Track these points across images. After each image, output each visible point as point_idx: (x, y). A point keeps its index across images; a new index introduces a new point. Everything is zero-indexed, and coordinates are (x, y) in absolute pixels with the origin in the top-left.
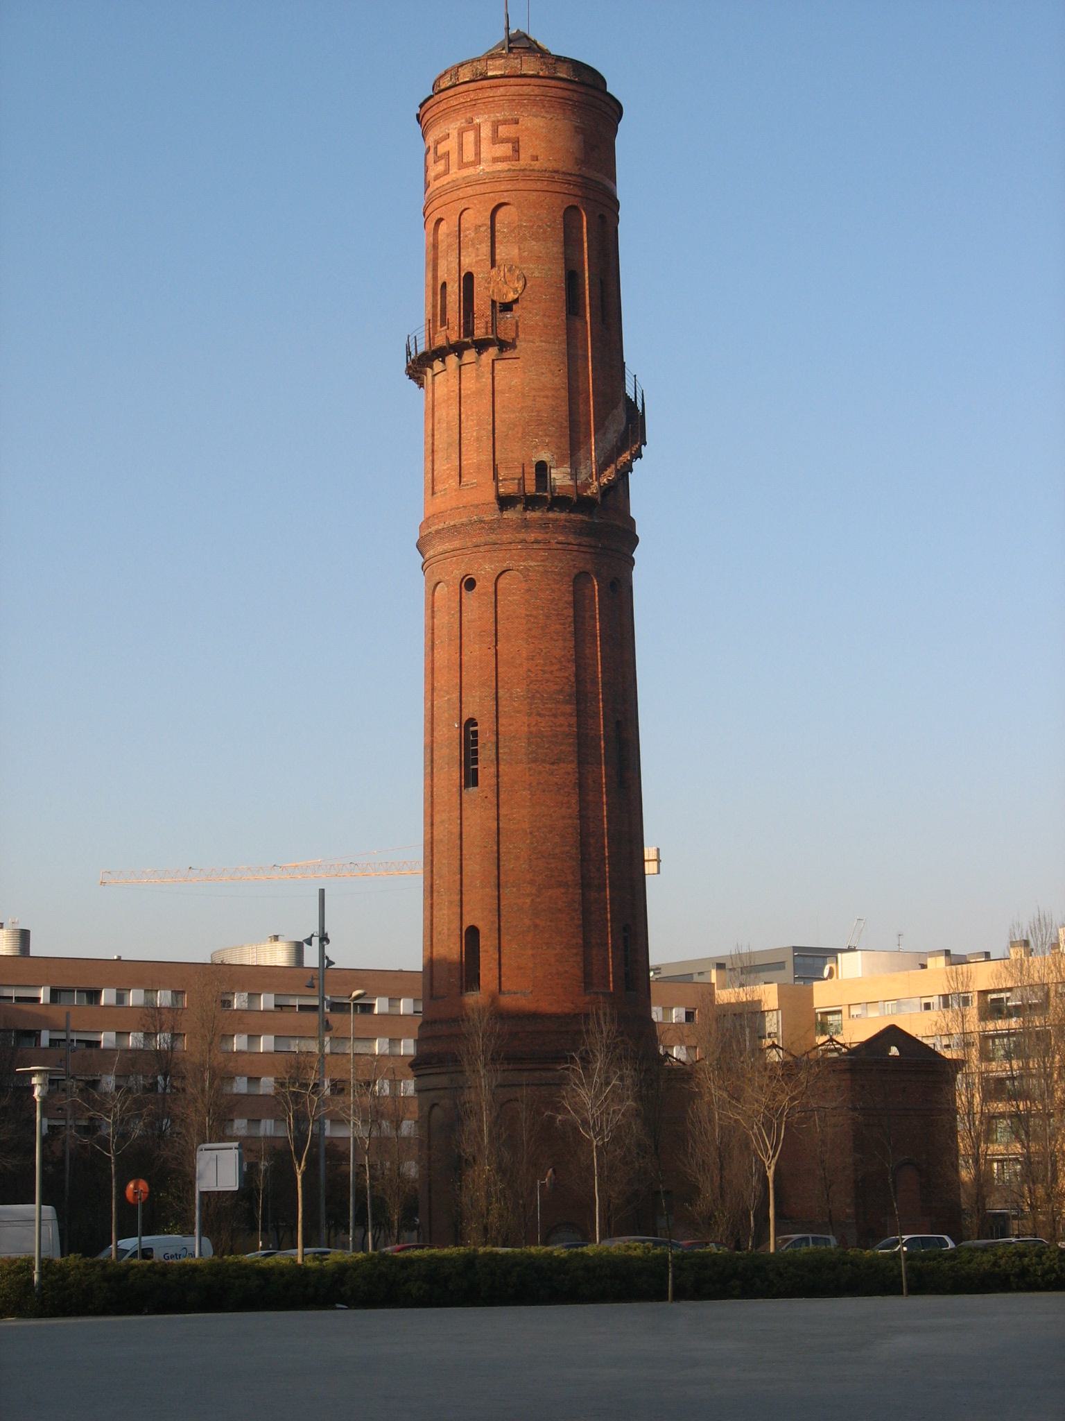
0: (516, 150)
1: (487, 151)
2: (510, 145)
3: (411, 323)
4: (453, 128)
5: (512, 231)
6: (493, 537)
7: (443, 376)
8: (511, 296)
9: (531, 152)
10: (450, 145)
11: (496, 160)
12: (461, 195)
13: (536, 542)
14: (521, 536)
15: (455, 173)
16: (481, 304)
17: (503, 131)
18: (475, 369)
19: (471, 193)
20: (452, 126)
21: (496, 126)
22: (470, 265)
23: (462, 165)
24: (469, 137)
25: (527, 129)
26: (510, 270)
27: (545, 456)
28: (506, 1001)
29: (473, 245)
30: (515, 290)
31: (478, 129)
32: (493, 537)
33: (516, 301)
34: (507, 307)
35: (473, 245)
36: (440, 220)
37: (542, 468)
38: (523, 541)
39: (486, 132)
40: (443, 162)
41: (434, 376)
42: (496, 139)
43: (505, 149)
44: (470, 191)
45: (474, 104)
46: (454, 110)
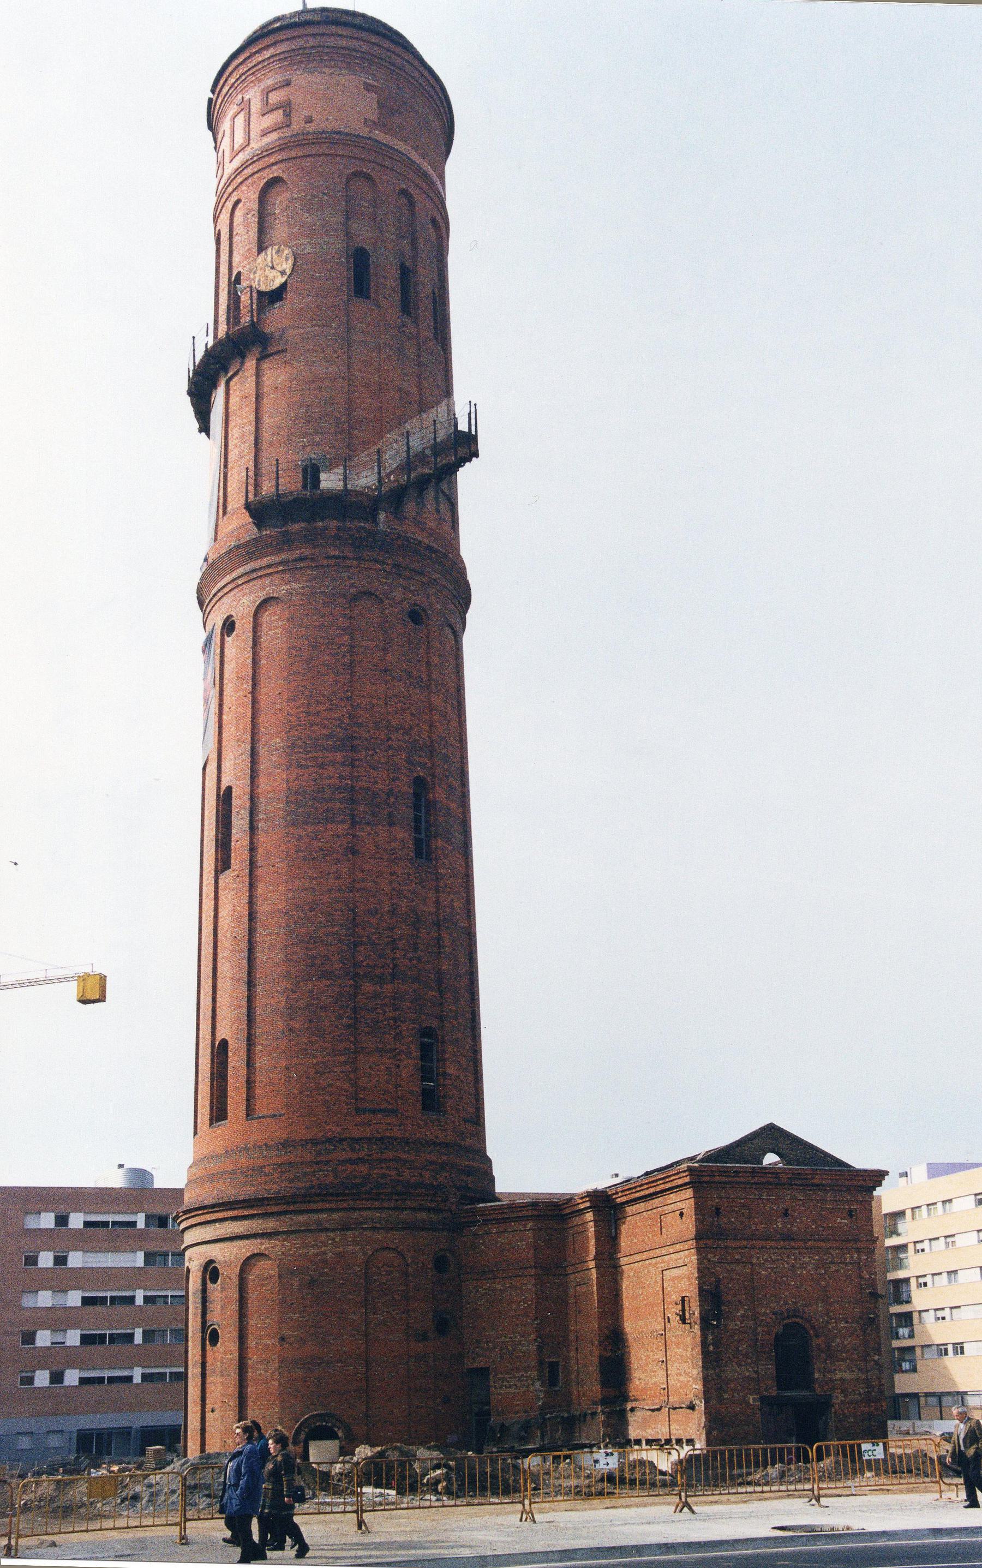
33: (284, 286)
37: (311, 473)
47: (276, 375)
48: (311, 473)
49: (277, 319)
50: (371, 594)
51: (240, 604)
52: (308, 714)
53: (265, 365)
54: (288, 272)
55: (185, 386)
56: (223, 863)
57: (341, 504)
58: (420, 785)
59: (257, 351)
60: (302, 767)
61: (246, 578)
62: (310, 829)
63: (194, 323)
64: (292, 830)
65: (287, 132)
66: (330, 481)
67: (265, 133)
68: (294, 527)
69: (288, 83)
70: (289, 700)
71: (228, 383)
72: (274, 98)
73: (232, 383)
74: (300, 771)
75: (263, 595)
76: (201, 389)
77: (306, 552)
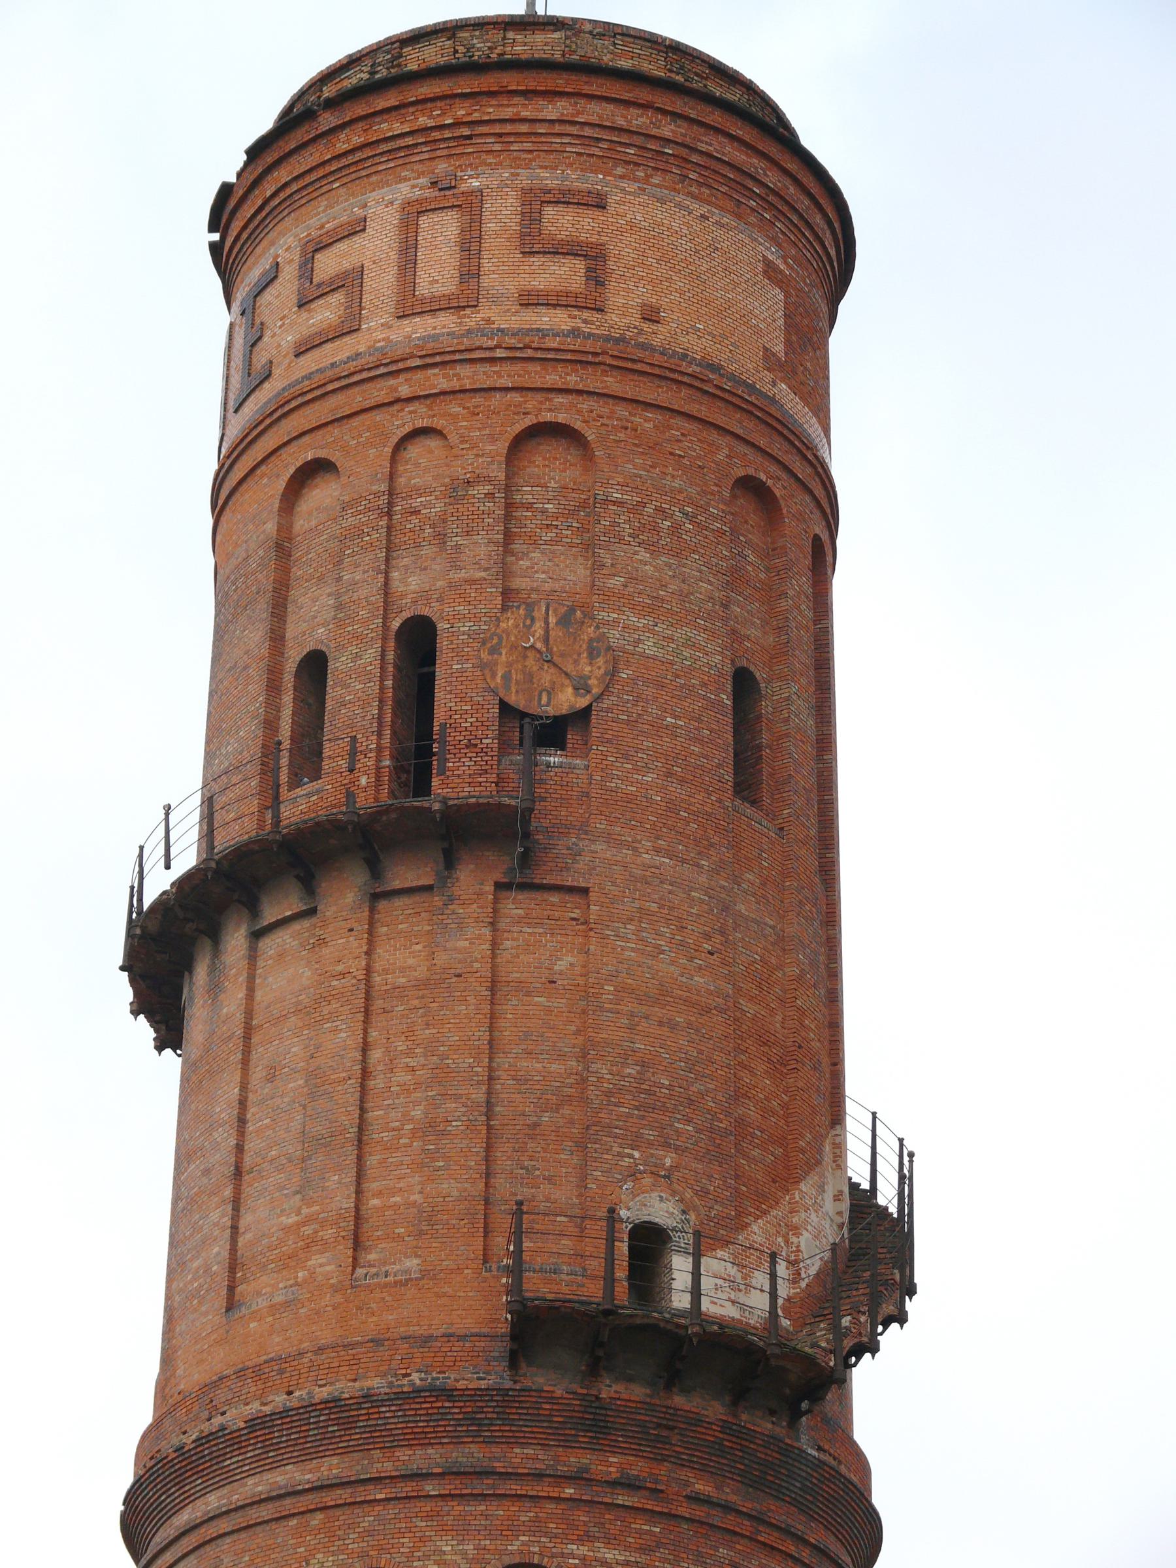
0: (596, 278)
1: (504, 272)
2: (579, 264)
3: (143, 783)
4: (382, 203)
5: (571, 513)
6: (471, 1454)
7: (279, 969)
8: (567, 700)
9: (642, 294)
10: (375, 248)
11: (529, 300)
12: (405, 391)
13: (629, 1484)
14: (576, 1460)
15: (383, 330)
16: (458, 700)
17: (559, 222)
18: (433, 939)
19: (443, 384)
20: (386, 193)
21: (535, 201)
22: (424, 596)
23: (410, 306)
24: (441, 233)
25: (632, 226)
26: (564, 621)
27: (660, 1209)
28: (537, 1287)
29: (441, 539)
30: (581, 687)
31: (471, 206)
32: (471, 1454)
33: (583, 716)
34: (553, 732)
35: (441, 539)
36: (315, 470)
37: (649, 1244)
38: (579, 1477)
39: (502, 216)
40: (337, 298)
41: (257, 935)
42: (533, 244)
43: (566, 274)
44: (440, 380)
45: (463, 137)
46: (397, 151)
59: (498, 865)
76: (165, 957)
77: (639, 1468)
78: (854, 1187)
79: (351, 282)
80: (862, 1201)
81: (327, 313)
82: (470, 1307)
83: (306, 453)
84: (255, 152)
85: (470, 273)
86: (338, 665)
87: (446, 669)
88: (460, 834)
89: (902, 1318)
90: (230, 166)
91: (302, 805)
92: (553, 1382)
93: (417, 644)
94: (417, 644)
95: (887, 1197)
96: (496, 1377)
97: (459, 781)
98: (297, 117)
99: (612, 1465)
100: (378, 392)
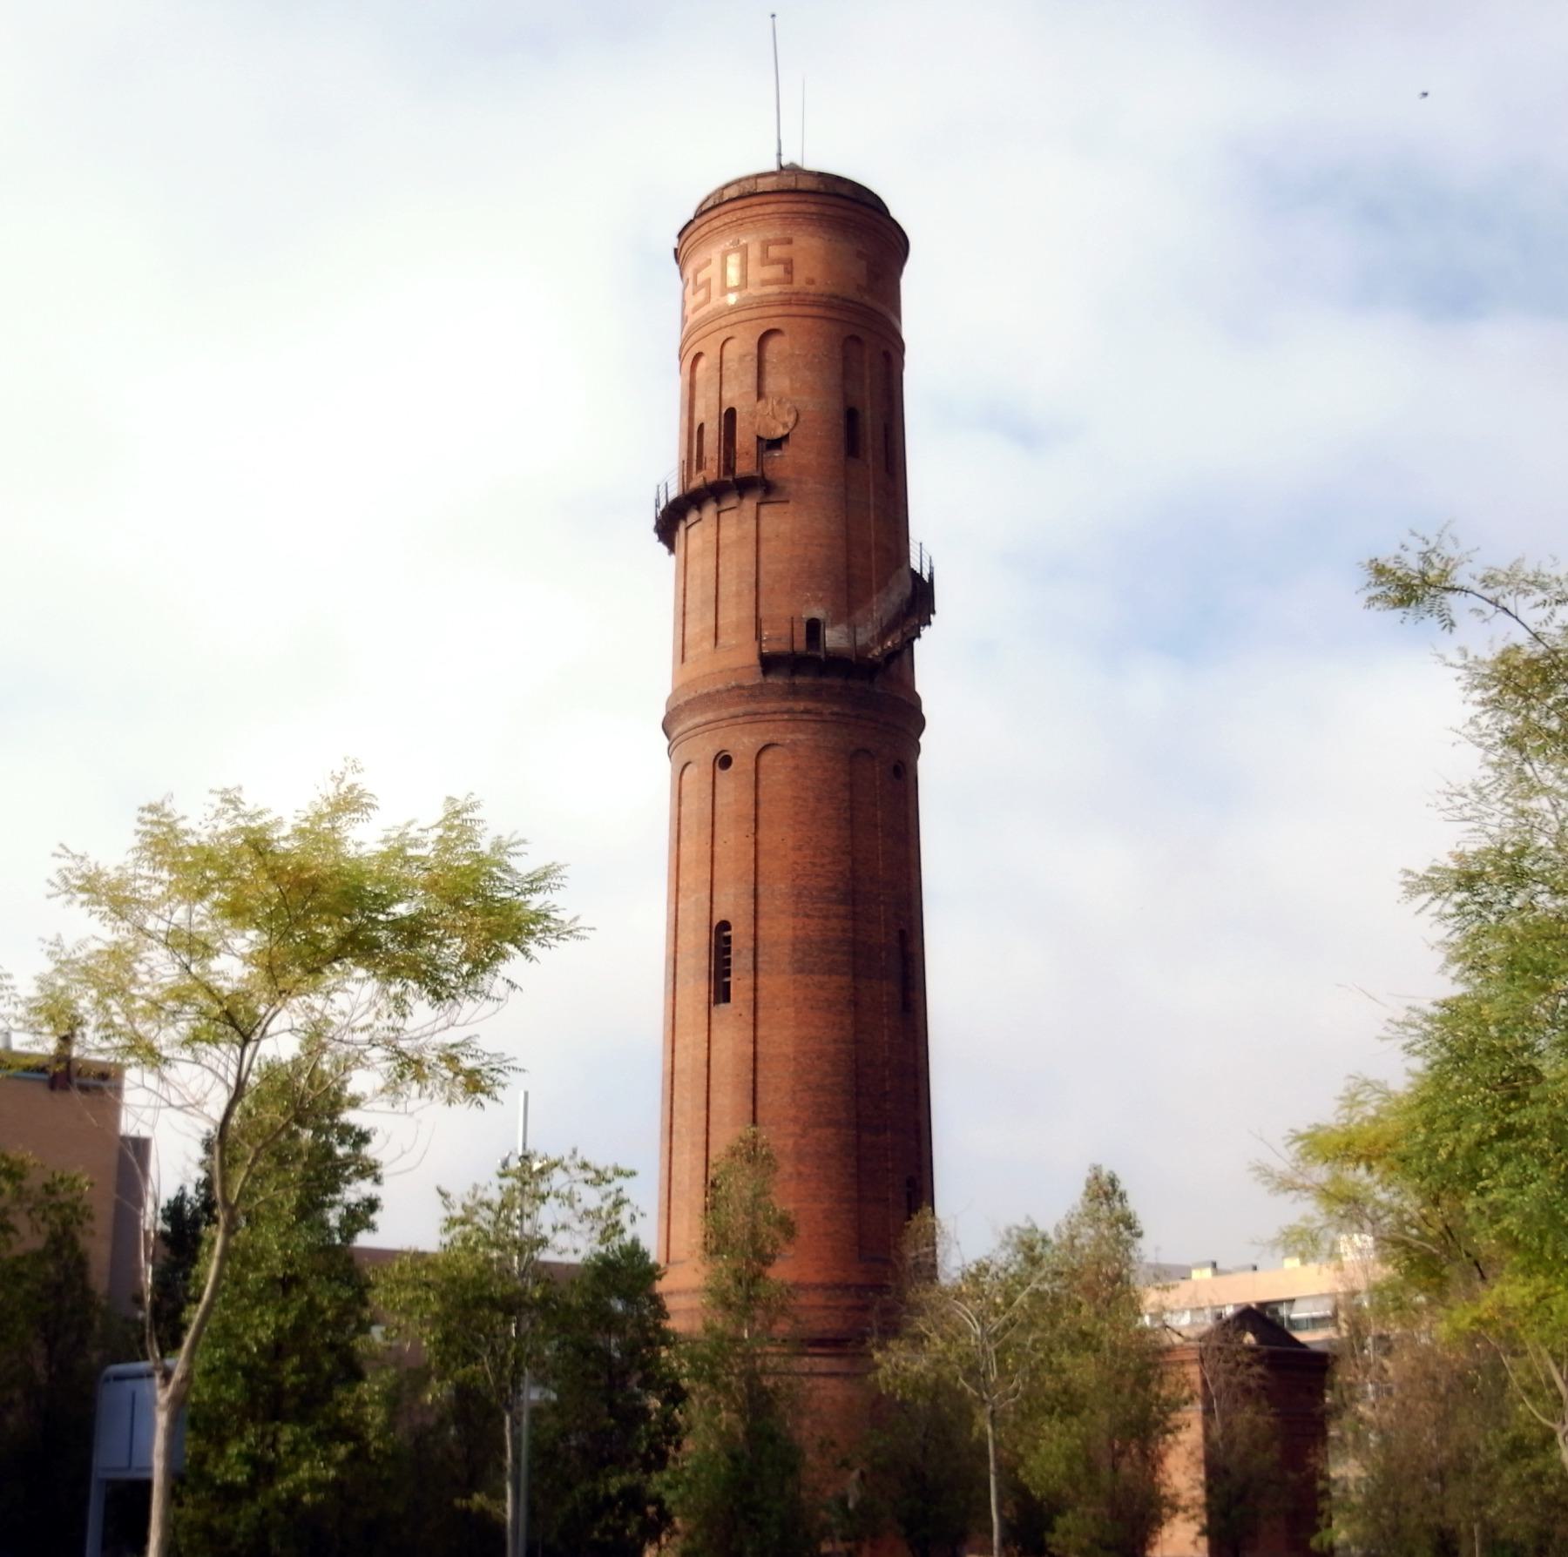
4: (715, 253)
7: (698, 532)
27: (818, 612)
30: (785, 425)
33: (785, 438)
34: (776, 444)
36: (698, 356)
37: (814, 628)
39: (754, 252)
47: (779, 523)
48: (814, 628)
49: (782, 464)
50: (868, 752)
51: (743, 743)
52: (814, 864)
53: (765, 510)
54: (790, 425)
55: (653, 523)
56: (721, 993)
57: (837, 664)
58: (902, 933)
59: (759, 494)
60: (808, 916)
61: (747, 718)
62: (817, 978)
63: (661, 471)
64: (799, 977)
65: (787, 288)
66: (834, 638)
67: (765, 283)
68: (798, 680)
69: (790, 242)
70: (793, 849)
71: (687, 528)
72: (774, 251)
73: (691, 531)
74: (807, 921)
75: (768, 739)
76: (669, 524)
77: (811, 705)
78: (913, 572)
79: (708, 282)
80: (916, 577)
81: (701, 295)
82: (749, 657)
83: (695, 351)
84: (680, 235)
85: (744, 276)
86: (706, 428)
87: (739, 424)
88: (743, 486)
89: (929, 623)
90: (674, 243)
91: (697, 481)
92: (776, 680)
93: (730, 416)
94: (730, 416)
95: (926, 577)
96: (759, 679)
97: (744, 467)
98: (701, 213)
99: (801, 706)
100: (715, 325)
